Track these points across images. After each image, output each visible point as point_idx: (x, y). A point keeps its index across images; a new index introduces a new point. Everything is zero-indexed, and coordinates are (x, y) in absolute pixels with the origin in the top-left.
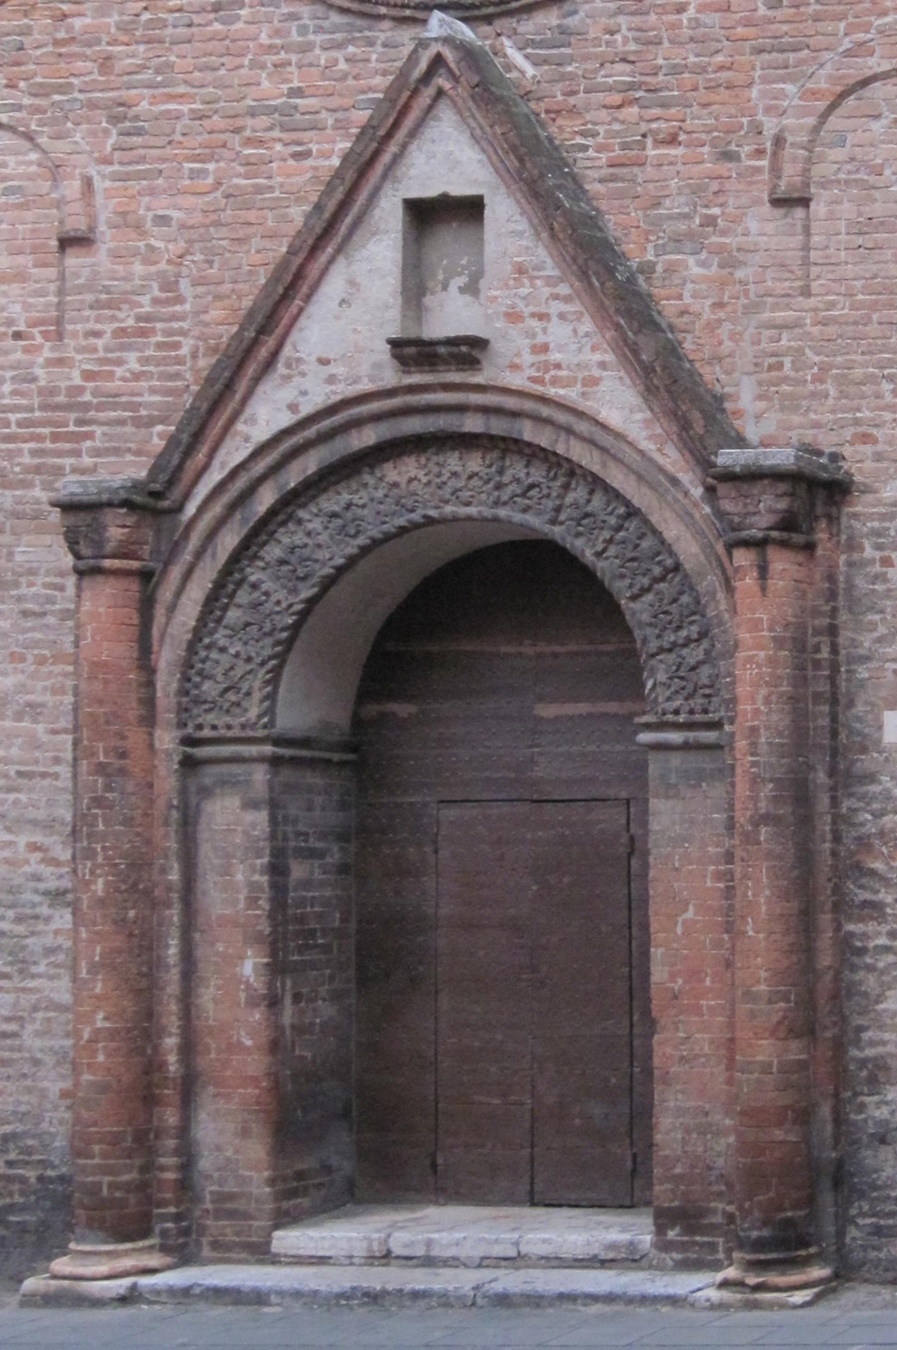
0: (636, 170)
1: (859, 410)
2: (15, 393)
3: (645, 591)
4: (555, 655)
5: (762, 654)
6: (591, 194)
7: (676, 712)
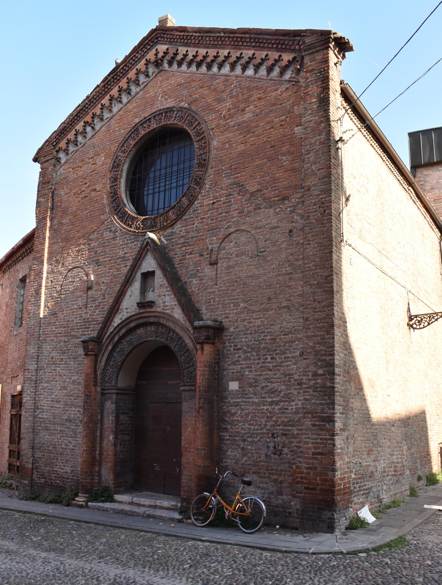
3: (182, 355)
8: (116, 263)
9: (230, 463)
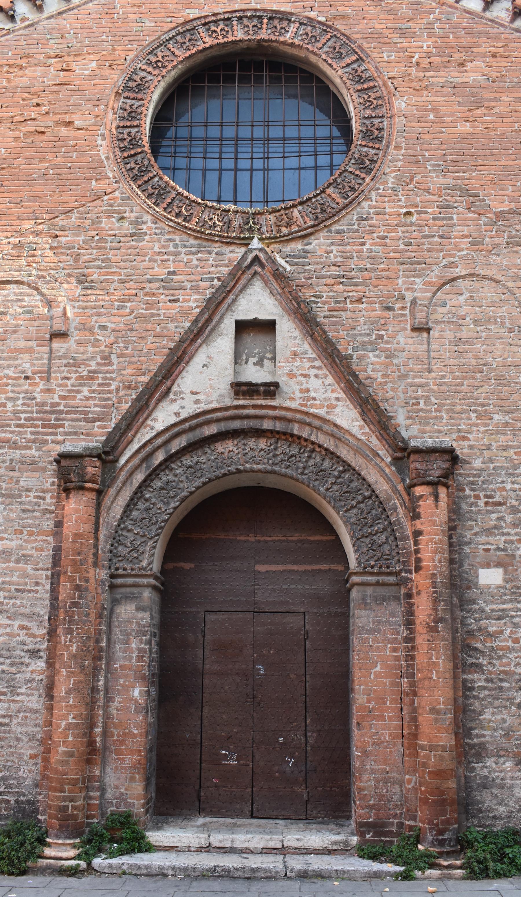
0: (342, 313)
1: (460, 425)
2: (24, 404)
3: (352, 507)
4: (266, 542)
5: (437, 538)
6: (321, 323)
7: (372, 567)
8: (143, 289)
9: (492, 737)
